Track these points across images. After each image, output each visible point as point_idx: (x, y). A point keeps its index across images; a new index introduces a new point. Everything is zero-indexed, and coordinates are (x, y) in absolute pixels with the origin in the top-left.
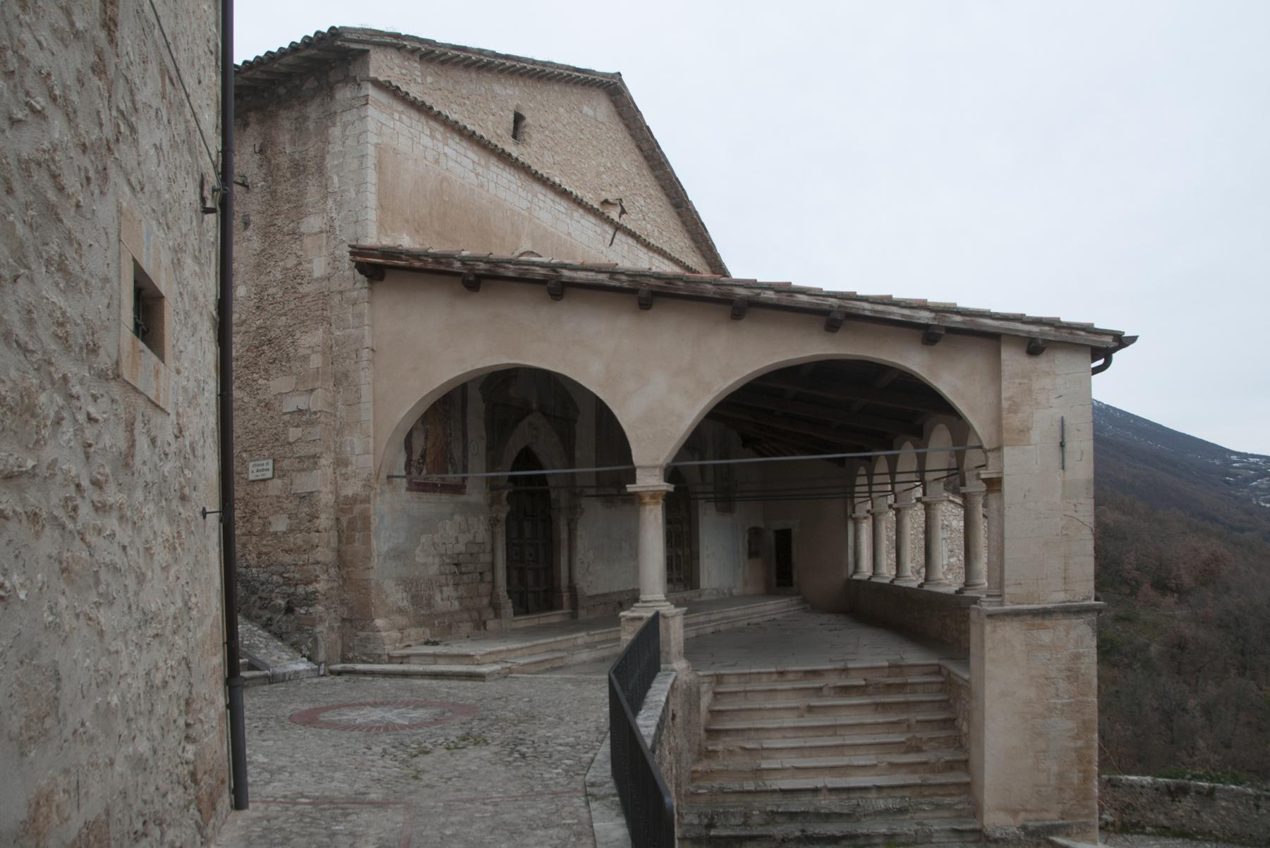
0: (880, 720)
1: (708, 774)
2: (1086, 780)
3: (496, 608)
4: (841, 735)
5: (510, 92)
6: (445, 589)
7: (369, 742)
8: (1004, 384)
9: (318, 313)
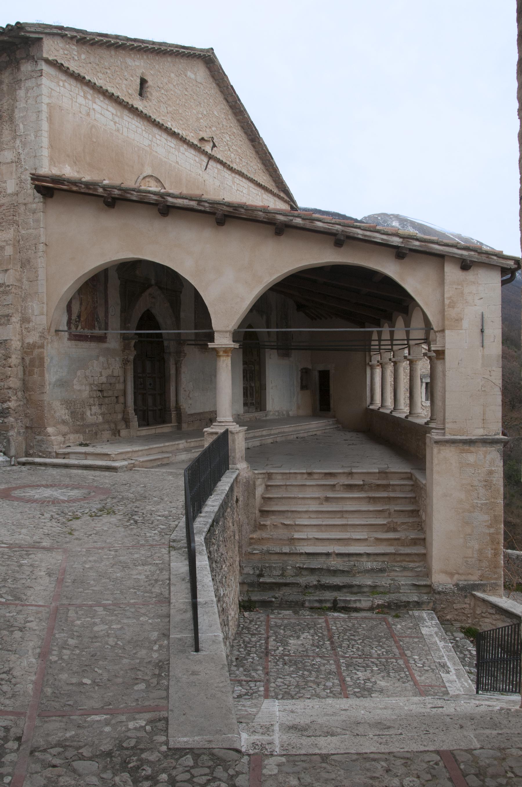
0: (371, 509)
1: (260, 540)
2: (496, 555)
3: (126, 421)
4: (346, 518)
5: (137, 63)
6: (93, 407)
7: (42, 511)
8: (446, 288)
9: (10, 218)
